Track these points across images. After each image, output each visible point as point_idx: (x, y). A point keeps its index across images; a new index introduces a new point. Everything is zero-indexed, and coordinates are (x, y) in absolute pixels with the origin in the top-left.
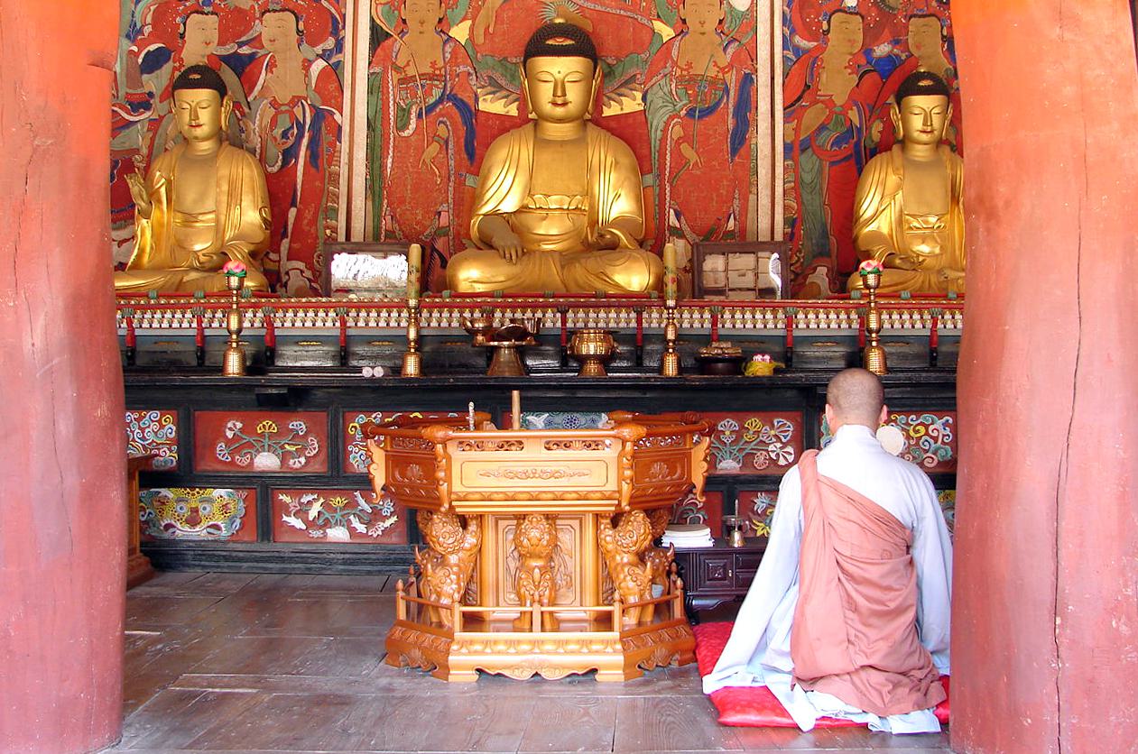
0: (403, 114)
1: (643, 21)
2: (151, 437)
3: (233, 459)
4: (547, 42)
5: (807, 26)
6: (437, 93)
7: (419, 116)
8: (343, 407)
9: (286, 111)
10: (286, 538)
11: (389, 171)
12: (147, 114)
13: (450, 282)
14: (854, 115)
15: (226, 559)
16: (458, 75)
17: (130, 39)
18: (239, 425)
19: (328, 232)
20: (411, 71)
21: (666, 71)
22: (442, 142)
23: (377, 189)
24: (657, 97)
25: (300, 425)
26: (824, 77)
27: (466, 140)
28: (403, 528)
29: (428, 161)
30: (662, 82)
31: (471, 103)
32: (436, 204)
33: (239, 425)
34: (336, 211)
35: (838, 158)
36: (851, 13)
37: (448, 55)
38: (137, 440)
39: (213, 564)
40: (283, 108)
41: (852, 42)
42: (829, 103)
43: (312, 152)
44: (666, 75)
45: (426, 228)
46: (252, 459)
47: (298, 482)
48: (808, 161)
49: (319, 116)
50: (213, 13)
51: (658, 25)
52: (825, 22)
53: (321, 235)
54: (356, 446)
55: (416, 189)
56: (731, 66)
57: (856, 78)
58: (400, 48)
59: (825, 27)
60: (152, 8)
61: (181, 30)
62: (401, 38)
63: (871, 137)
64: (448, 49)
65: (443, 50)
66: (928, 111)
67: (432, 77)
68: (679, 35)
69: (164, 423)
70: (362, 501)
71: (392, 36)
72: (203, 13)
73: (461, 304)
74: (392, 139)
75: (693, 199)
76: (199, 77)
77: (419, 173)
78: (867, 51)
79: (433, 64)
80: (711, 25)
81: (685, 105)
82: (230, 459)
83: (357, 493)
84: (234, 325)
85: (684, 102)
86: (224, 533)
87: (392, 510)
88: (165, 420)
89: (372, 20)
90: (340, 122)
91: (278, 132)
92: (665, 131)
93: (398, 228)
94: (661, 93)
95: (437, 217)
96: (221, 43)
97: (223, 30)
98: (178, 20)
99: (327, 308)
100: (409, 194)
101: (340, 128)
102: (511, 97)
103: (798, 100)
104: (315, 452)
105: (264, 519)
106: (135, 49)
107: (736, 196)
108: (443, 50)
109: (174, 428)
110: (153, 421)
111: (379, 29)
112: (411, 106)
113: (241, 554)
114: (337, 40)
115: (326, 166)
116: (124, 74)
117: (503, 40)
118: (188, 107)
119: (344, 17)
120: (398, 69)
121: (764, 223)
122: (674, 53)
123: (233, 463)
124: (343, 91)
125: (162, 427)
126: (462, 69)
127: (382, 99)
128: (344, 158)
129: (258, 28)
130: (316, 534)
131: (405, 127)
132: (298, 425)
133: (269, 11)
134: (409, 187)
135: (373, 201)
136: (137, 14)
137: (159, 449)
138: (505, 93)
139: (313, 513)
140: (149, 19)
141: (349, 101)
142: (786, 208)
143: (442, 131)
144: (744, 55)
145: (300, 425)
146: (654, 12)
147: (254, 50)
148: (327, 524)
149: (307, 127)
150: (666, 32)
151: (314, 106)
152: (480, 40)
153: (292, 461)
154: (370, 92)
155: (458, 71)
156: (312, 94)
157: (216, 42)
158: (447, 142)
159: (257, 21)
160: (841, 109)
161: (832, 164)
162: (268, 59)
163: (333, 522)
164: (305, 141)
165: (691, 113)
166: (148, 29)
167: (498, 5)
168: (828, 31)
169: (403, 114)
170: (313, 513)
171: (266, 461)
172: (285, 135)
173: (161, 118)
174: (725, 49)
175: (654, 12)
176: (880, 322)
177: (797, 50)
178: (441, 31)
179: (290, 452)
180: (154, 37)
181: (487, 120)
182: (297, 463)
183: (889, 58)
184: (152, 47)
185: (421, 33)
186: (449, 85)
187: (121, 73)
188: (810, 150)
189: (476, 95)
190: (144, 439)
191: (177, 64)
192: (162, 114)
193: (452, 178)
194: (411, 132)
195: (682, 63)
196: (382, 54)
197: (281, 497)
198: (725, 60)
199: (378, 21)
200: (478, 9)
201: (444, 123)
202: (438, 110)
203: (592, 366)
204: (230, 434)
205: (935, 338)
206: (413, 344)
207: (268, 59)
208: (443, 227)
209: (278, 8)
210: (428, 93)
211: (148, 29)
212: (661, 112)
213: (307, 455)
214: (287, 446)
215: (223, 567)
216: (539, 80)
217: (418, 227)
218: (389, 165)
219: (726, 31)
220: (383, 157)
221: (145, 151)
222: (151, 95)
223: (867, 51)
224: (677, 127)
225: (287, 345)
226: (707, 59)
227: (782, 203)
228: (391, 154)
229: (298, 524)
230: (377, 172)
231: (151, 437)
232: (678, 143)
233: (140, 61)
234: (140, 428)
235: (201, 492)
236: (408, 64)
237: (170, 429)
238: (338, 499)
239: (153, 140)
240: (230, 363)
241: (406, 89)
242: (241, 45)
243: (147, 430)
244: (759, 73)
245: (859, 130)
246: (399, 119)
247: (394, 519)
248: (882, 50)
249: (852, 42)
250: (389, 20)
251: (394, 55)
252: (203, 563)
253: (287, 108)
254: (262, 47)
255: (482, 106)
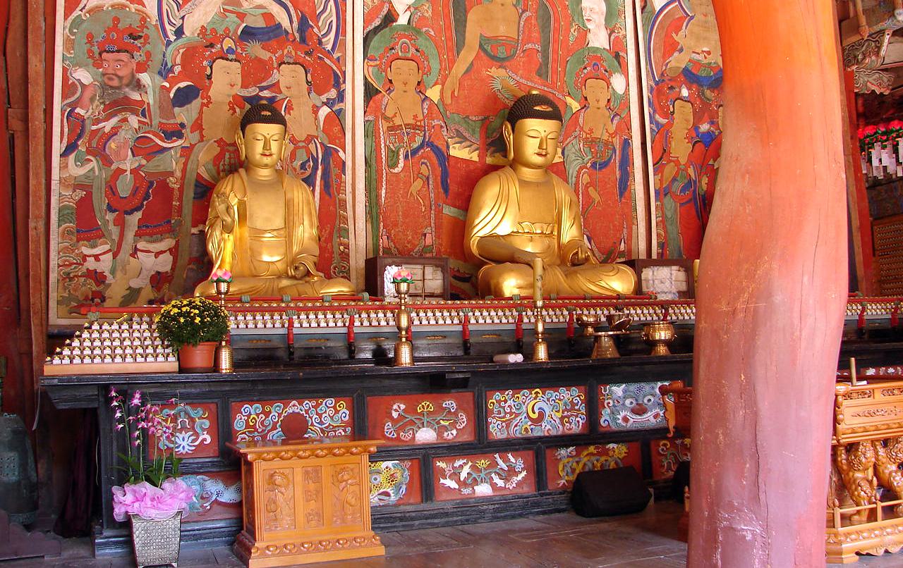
0: (393, 155)
1: (559, 96)
2: (327, 421)
3: (398, 435)
4: (535, 108)
5: (662, 108)
6: (419, 140)
7: (406, 157)
8: (486, 387)
9: (303, 147)
10: (444, 496)
11: (383, 199)
12: (180, 142)
13: (495, 288)
14: (691, 171)
15: (401, 519)
16: (433, 127)
17: (162, 76)
18: (403, 407)
19: (342, 248)
20: (398, 121)
21: (576, 134)
22: (424, 179)
23: (374, 214)
24: (571, 151)
25: (452, 404)
26: (673, 143)
27: (442, 179)
28: (533, 479)
29: (415, 194)
30: (574, 142)
31: (444, 149)
32: (422, 228)
33: (403, 407)
34: (347, 231)
35: (684, 201)
36: (686, 101)
37: (426, 111)
38: (315, 424)
39: (389, 525)
40: (301, 144)
41: (687, 121)
42: (677, 163)
43: (325, 182)
44: (576, 137)
45: (415, 246)
46: (414, 434)
47: (453, 450)
48: (668, 201)
49: (328, 152)
50: (236, 60)
51: (569, 100)
52: (671, 106)
53: (336, 250)
54: (494, 418)
55: (405, 215)
56: (616, 133)
57: (690, 145)
58: (389, 103)
59: (672, 110)
60: (181, 51)
61: (208, 72)
62: (389, 94)
63: (701, 187)
64: (426, 106)
65: (422, 106)
66: (268, 137)
67: (414, 127)
68: (583, 108)
69: (338, 409)
70: (500, 461)
71: (381, 92)
72: (227, 59)
73: (249, 309)
74: (385, 175)
75: (598, 228)
76: (270, 114)
77: (408, 203)
78: (696, 127)
79: (415, 117)
80: (603, 103)
81: (590, 159)
82: (396, 436)
83: (497, 456)
84: (404, 322)
85: (589, 157)
86: (393, 498)
87: (523, 466)
88: (339, 406)
89: (365, 78)
90: (343, 158)
91: (297, 164)
92: (578, 177)
93: (393, 246)
94: (573, 150)
95: (423, 238)
96: (244, 86)
97: (245, 75)
98: (205, 63)
99: (263, 311)
100: (401, 219)
101: (344, 163)
102: (473, 147)
103: (660, 160)
104: (464, 425)
105: (426, 483)
106: (167, 85)
107: (625, 226)
108: (422, 106)
109: (348, 412)
110: (328, 407)
111: (371, 87)
112: (400, 148)
113: (414, 514)
114: (338, 91)
115: (336, 193)
116: (157, 106)
117: (465, 102)
118: (263, 138)
119: (344, 73)
120: (387, 119)
121: (642, 246)
122: (581, 121)
123: (398, 438)
124: (345, 134)
125: (337, 412)
126: (436, 122)
127: (376, 142)
128: (349, 188)
129: (276, 76)
130: (467, 491)
131: (396, 165)
132: (450, 404)
133: (284, 63)
134: (401, 213)
135: (372, 223)
136: (167, 55)
137: (335, 431)
138: (468, 143)
139: (463, 475)
140: (178, 61)
141: (351, 142)
142: (658, 235)
143: (424, 169)
144: (623, 126)
145: (452, 404)
146: (566, 90)
147: (274, 94)
148: (475, 482)
149: (320, 161)
150: (575, 106)
151: (323, 144)
152: (448, 101)
153: (446, 434)
154: (366, 136)
155: (434, 124)
156: (321, 134)
157: (240, 84)
158: (428, 178)
159: (275, 71)
160: (684, 167)
161: (681, 205)
162: (286, 102)
163: (479, 480)
164: (319, 172)
165: (594, 165)
166: (178, 69)
167: (460, 75)
168: (673, 112)
169: (393, 155)
170: (463, 475)
171: (426, 435)
172: (303, 166)
173: (192, 146)
174: (612, 120)
175: (566, 90)
176: (411, 321)
177: (657, 123)
178: (420, 91)
179: (444, 426)
180: (184, 75)
181: (457, 163)
182: (451, 435)
183: (708, 133)
184: (182, 85)
185: (405, 92)
186: (427, 134)
187: (154, 105)
188: (669, 195)
189: (447, 143)
190: (321, 423)
191: (205, 101)
192: (193, 143)
193: (433, 208)
194: (400, 169)
195: (586, 129)
196: (374, 105)
197: (438, 464)
198: (612, 128)
199: (370, 80)
200: (446, 77)
201: (423, 163)
202: (420, 153)
203: (662, 348)
204: (395, 415)
205: (291, 336)
206: (540, 335)
207: (286, 102)
208: (428, 246)
209: (292, 61)
210: (412, 140)
211: (178, 69)
212: (575, 163)
213: (458, 429)
214: (441, 422)
215: (399, 527)
216: (529, 136)
217: (409, 246)
218: (383, 195)
219: (612, 108)
220: (378, 188)
221: (178, 174)
222: (183, 125)
223: (696, 127)
224: (586, 175)
225: (419, 339)
226: (603, 128)
227: (655, 232)
228: (384, 186)
229: (451, 484)
230: (374, 200)
231: (327, 421)
232: (587, 187)
233: (172, 95)
234: (317, 414)
235: (372, 465)
236: (395, 116)
237: (344, 413)
238: (483, 461)
239: (185, 164)
240: (403, 355)
241: (395, 135)
242: (262, 89)
243: (324, 416)
244: (633, 139)
245: (695, 182)
246: (389, 159)
247: (524, 473)
248: (704, 127)
249: (687, 121)
250: (378, 79)
251: (383, 107)
252: (381, 525)
253: (304, 144)
254: (281, 92)
255: (453, 152)
